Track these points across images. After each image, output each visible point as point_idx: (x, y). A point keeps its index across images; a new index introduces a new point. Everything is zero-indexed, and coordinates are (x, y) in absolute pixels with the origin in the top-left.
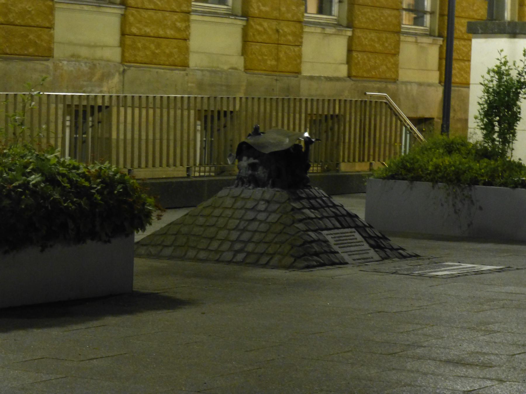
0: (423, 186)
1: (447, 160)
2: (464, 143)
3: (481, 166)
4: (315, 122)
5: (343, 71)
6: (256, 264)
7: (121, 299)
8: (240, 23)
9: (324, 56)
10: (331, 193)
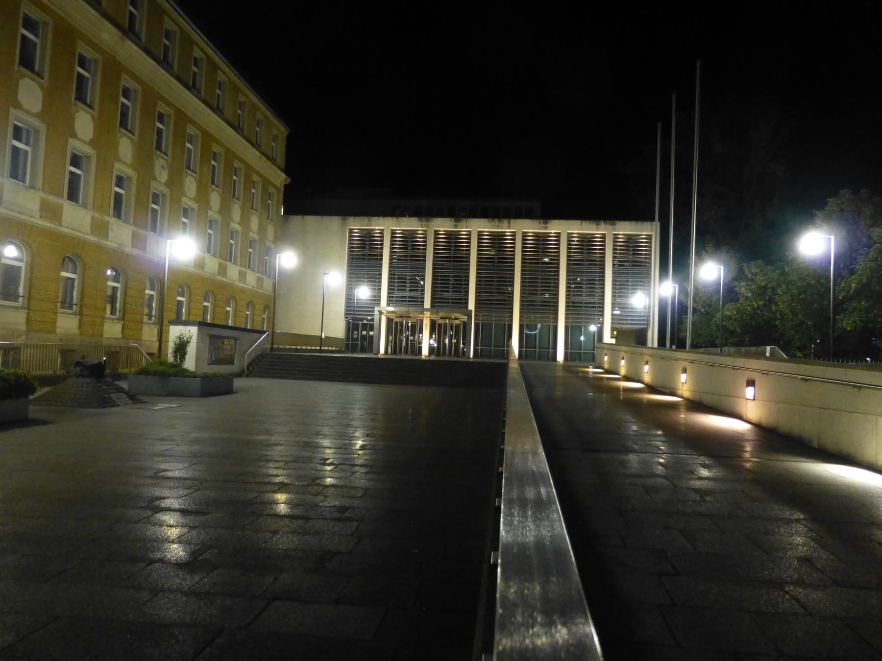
1: (160, 368)
3: (173, 370)
4: (108, 354)
5: (120, 336)
7: (22, 422)
9: (112, 330)
10: (114, 380)
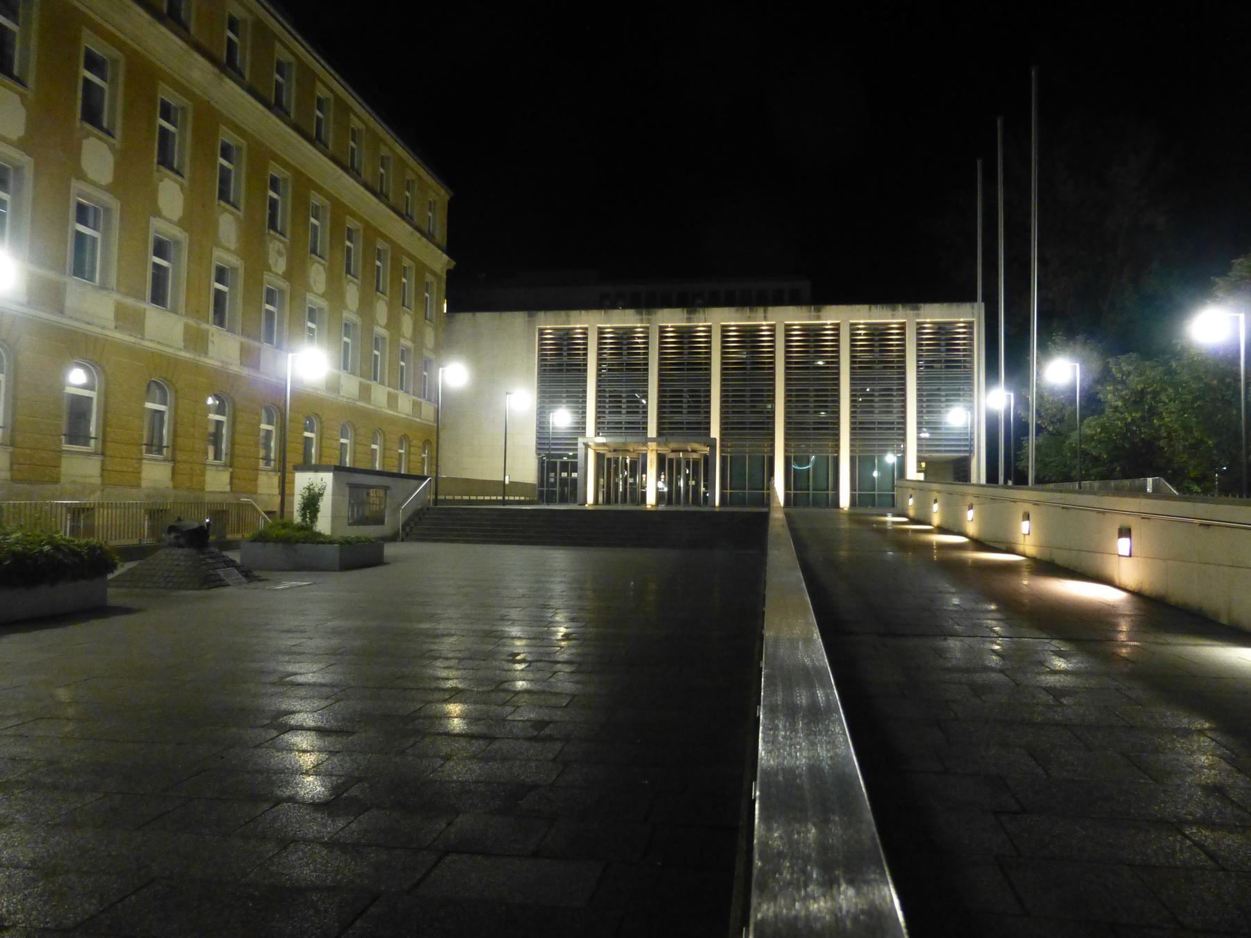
0: (270, 546)
1: (283, 532)
2: (292, 523)
5: (228, 489)
6: (179, 588)
7: (99, 610)
8: (171, 464)
9: (217, 481)
